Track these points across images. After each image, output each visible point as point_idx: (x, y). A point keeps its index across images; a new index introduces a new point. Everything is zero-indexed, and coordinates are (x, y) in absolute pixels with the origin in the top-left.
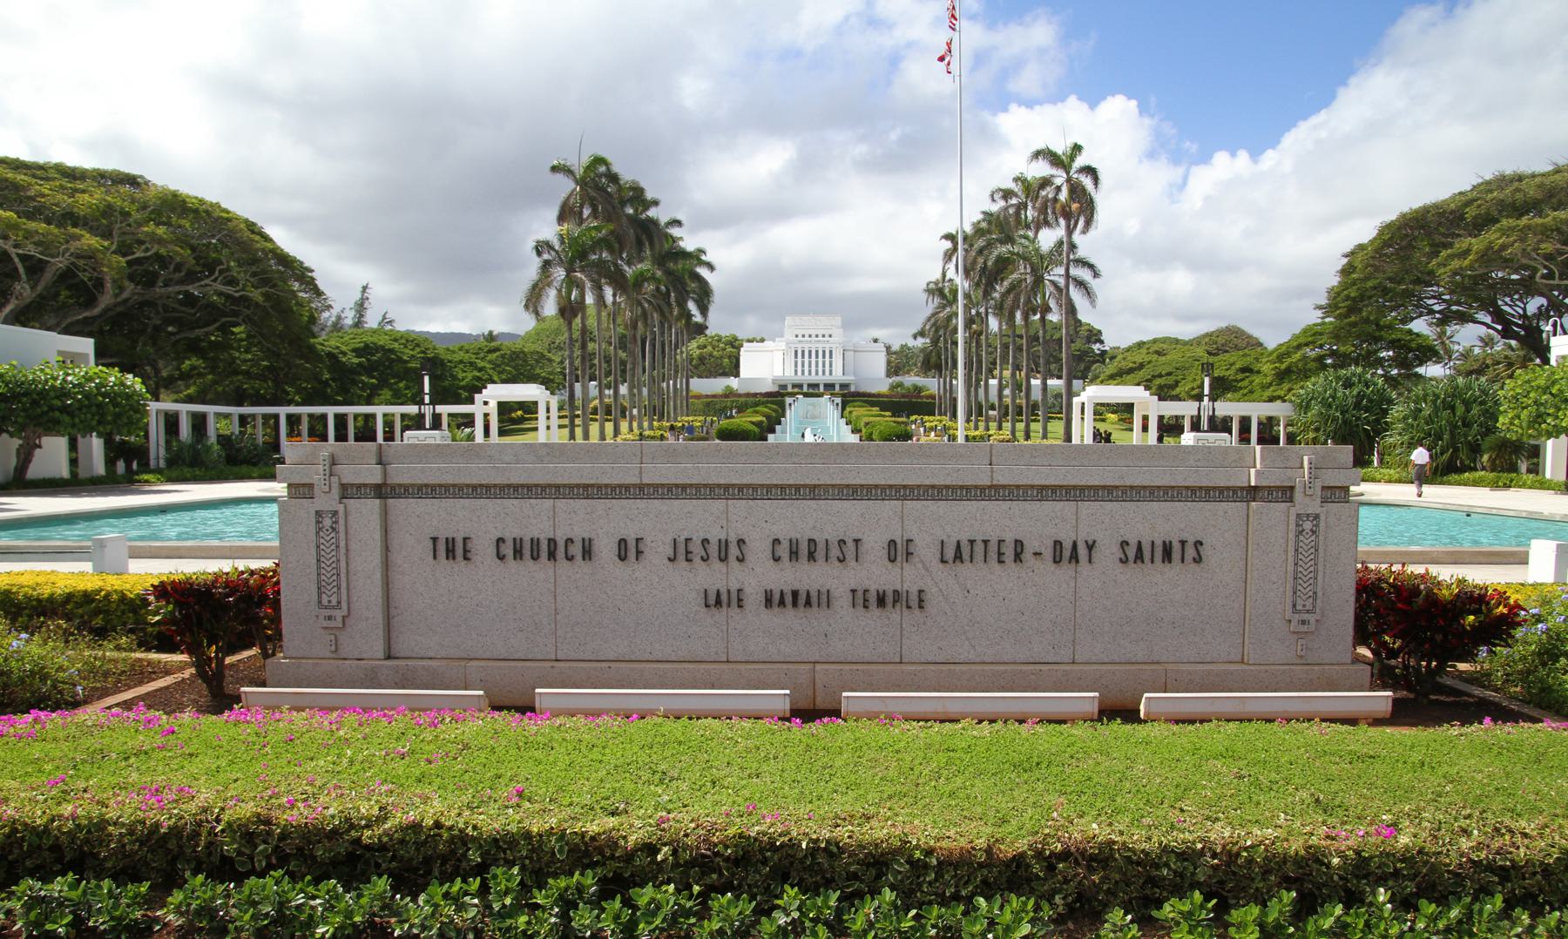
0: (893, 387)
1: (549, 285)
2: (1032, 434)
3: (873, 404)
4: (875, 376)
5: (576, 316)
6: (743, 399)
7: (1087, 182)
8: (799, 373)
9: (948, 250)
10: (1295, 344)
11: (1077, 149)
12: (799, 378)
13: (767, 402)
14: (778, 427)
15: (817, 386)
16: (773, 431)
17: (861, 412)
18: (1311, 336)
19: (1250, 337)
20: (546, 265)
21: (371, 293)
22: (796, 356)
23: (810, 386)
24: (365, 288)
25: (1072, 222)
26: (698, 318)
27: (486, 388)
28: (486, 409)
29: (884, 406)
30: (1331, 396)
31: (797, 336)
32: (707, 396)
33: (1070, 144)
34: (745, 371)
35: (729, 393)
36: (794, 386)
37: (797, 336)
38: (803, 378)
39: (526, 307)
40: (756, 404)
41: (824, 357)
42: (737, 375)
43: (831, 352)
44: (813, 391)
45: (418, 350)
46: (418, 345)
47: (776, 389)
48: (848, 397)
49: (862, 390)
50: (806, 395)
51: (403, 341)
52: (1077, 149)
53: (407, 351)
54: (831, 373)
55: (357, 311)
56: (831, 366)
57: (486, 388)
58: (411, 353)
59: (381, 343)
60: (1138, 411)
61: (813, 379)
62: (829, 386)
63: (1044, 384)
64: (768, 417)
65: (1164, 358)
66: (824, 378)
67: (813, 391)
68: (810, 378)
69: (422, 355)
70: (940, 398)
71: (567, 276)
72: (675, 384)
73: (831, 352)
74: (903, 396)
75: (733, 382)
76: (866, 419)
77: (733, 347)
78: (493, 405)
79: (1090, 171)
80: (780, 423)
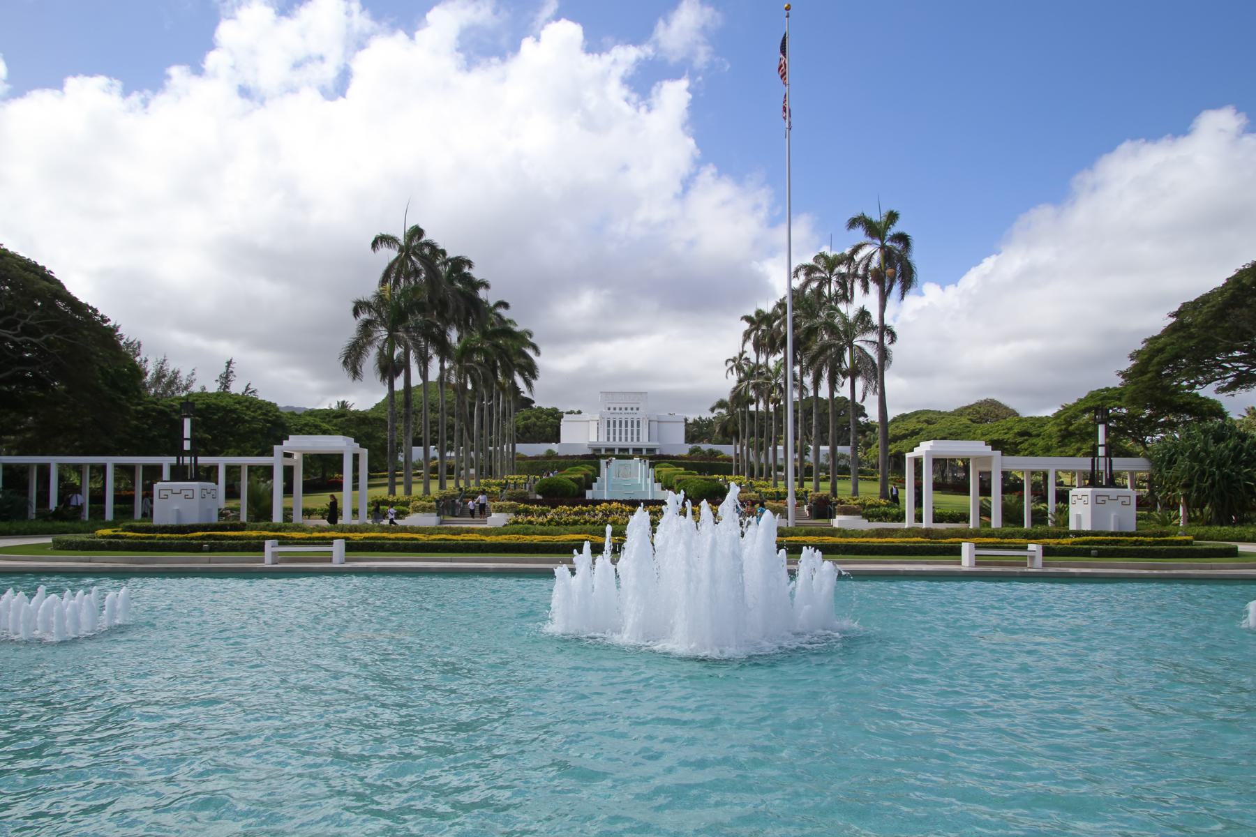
0: (692, 451)
1: (371, 343)
2: (838, 492)
3: (678, 465)
4: (676, 443)
5: (398, 374)
6: (562, 461)
7: (898, 246)
8: (611, 439)
9: (746, 331)
10: (1083, 407)
11: (893, 217)
12: (611, 444)
13: (584, 463)
14: (598, 478)
15: (627, 450)
16: (590, 488)
17: (666, 470)
18: (1101, 400)
19: (1006, 408)
20: (367, 328)
21: (234, 367)
22: (609, 426)
23: (620, 450)
24: (229, 363)
25: (887, 285)
26: (526, 394)
27: (287, 439)
28: (288, 462)
29: (687, 467)
30: (1203, 450)
31: (609, 409)
32: (531, 458)
33: (885, 212)
34: (564, 438)
35: (551, 455)
36: (607, 450)
37: (609, 409)
39: (345, 363)
40: (575, 465)
41: (626, 426)
42: (558, 440)
43: (638, 422)
44: (624, 454)
45: (259, 412)
46: (260, 408)
47: (590, 452)
48: (655, 458)
49: (665, 453)
50: (618, 457)
51: (247, 404)
52: (893, 217)
53: (248, 412)
54: (638, 440)
55: (222, 383)
56: (638, 434)
57: (287, 439)
58: (253, 414)
59: (223, 404)
60: (975, 467)
61: (623, 444)
62: (638, 451)
63: (834, 450)
64: (586, 475)
65: (932, 426)
66: (632, 443)
67: (624, 454)
68: (620, 443)
69: (264, 417)
71: (390, 335)
72: (508, 448)
73: (638, 422)
74: (702, 459)
75: (554, 447)
76: (677, 477)
77: (555, 418)
78: (297, 461)
79: (903, 238)
80: (596, 481)
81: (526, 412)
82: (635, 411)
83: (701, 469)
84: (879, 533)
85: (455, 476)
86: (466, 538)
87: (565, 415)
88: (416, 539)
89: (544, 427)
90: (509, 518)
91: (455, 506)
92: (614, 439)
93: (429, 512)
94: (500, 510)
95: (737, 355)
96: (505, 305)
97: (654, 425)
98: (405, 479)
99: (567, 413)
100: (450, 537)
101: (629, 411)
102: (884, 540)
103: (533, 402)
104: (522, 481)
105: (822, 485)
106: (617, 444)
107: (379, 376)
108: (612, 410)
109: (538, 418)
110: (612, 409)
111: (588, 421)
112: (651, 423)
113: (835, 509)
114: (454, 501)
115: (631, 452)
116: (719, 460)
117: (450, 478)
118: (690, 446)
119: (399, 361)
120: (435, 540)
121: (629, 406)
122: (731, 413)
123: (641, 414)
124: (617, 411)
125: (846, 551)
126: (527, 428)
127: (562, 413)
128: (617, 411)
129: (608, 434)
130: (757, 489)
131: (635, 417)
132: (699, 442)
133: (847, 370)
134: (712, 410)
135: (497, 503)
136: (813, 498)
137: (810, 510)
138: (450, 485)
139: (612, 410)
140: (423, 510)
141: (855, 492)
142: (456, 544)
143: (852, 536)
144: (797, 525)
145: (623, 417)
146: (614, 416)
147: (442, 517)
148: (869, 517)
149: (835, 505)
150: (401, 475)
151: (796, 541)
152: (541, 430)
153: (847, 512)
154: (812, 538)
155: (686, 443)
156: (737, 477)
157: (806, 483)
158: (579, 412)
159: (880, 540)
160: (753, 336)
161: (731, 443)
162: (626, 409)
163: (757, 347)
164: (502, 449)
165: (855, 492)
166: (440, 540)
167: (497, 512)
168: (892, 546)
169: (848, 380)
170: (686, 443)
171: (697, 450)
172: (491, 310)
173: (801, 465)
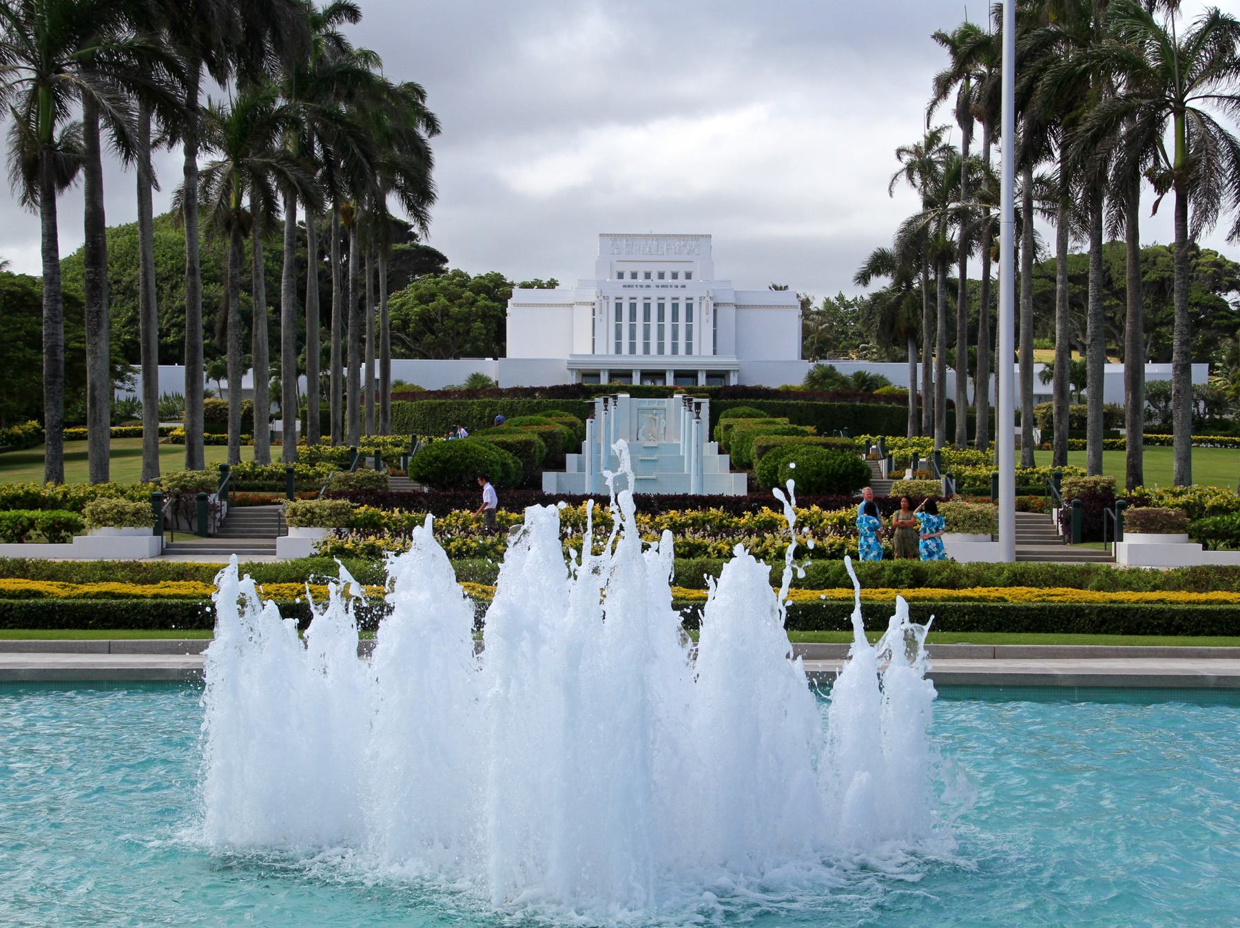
3: (776, 412)
5: (65, 181)
12: (624, 360)
15: (661, 375)
16: (560, 466)
23: (645, 374)
31: (621, 276)
35: (479, 387)
36: (613, 375)
37: (621, 276)
38: (633, 359)
40: (533, 410)
43: (689, 308)
47: (572, 380)
49: (751, 383)
50: (637, 393)
54: (689, 350)
61: (654, 361)
66: (675, 359)
70: (918, 400)
72: (370, 370)
73: (689, 308)
74: (838, 395)
75: (488, 367)
76: (762, 440)
77: (494, 299)
81: (424, 282)
82: (682, 279)
83: (827, 421)
84: (1198, 579)
85: (228, 436)
86: (167, 591)
87: (516, 291)
88: (37, 594)
89: (467, 319)
90: (321, 539)
91: (207, 510)
92: (661, 350)
93: (132, 524)
94: (309, 519)
95: (922, 142)
96: (353, 14)
97: (728, 315)
98: (94, 444)
99: (525, 286)
100: (129, 588)
101: (668, 280)
102: (1203, 596)
103: (445, 260)
104: (400, 449)
105: (1108, 457)
106: (640, 360)
107: (20, 188)
108: (627, 279)
109: (452, 298)
110: (627, 276)
111: (571, 305)
112: (719, 310)
113: (1121, 518)
114: (204, 498)
115: (670, 381)
116: (878, 398)
117: (218, 442)
118: (809, 366)
119: (68, 147)
120: (85, 596)
121: (668, 269)
122: (903, 278)
123: (694, 289)
124: (641, 280)
125: (1103, 622)
126: (427, 321)
127: (512, 285)
128: (641, 280)
129: (618, 335)
130: (954, 468)
131: (682, 295)
132: (836, 356)
133: (1170, 173)
134: (863, 278)
135: (301, 504)
136: (1075, 490)
137: (1065, 520)
138: (215, 456)
139: (627, 279)
140: (119, 519)
141: (1184, 477)
142: (135, 606)
143: (1127, 586)
144: (1020, 556)
145: (682, 295)
146: (647, 293)
147: (166, 537)
148: (1206, 538)
149: (1123, 507)
150: (80, 437)
151: (982, 599)
152: (461, 327)
153: (1150, 525)
154: (1025, 589)
155: (803, 358)
156: (915, 439)
157: (1071, 455)
158: (552, 284)
159: (1194, 596)
160: (955, 90)
161: (904, 360)
162: (675, 276)
163: (965, 116)
164: (355, 374)
165: (1184, 477)
166: (98, 595)
167: (301, 524)
168: (1220, 612)
169: (1171, 196)
170: (803, 358)
171: (830, 374)
172: (318, 22)
173: (1061, 410)
